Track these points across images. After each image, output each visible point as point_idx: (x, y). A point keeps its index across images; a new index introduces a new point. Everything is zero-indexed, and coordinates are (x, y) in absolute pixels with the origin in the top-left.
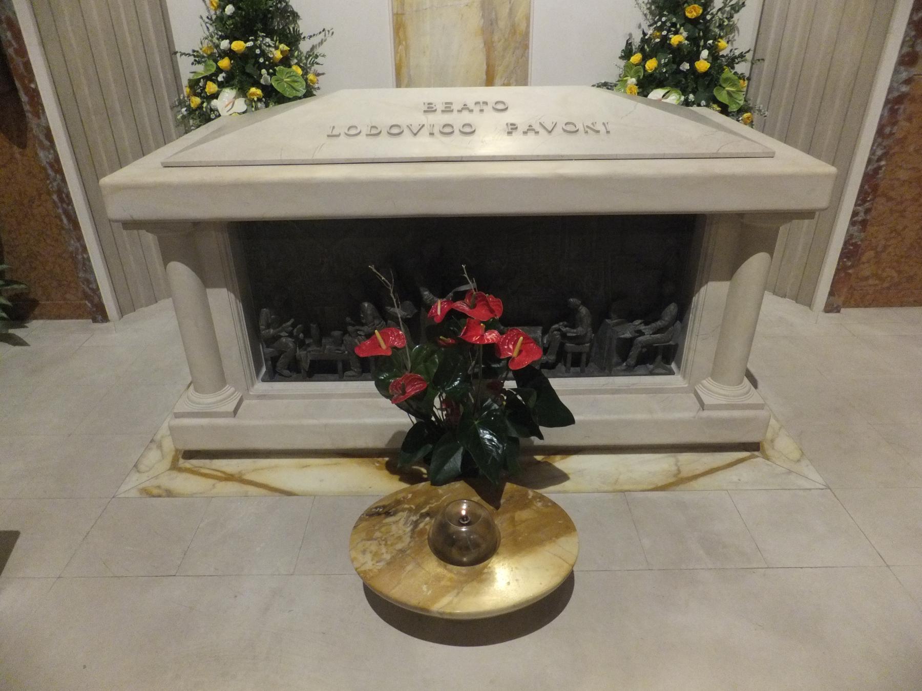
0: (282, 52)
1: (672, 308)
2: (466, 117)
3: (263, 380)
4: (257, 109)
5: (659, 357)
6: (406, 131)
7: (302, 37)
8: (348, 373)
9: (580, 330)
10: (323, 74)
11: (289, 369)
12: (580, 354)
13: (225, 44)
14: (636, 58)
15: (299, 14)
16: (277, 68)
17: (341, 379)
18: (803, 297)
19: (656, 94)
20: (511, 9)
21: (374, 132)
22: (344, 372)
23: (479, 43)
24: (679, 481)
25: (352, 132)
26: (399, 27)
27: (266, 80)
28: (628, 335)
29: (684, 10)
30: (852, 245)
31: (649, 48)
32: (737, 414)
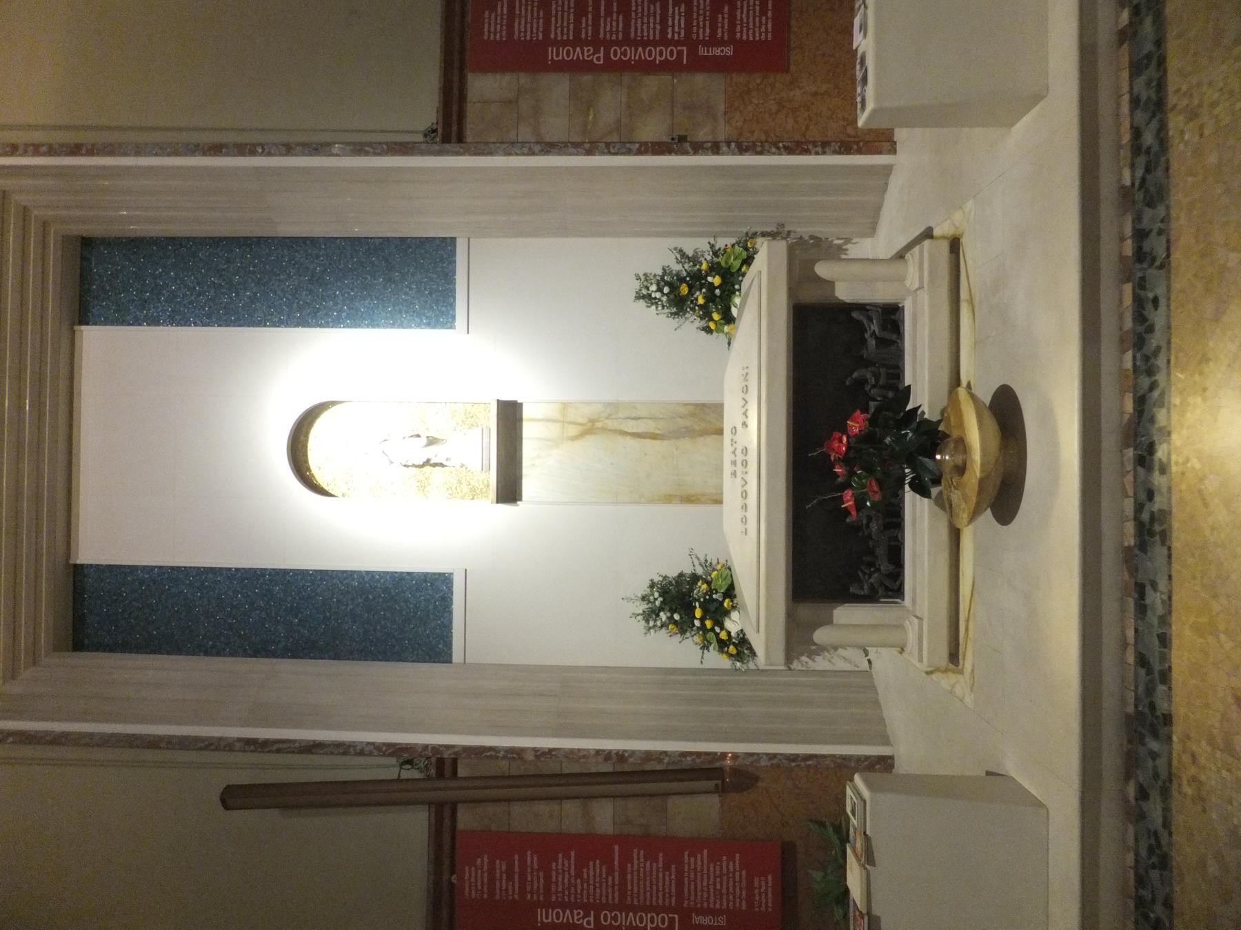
0: (703, 584)
1: (855, 315)
2: (738, 452)
3: (903, 600)
4: (737, 604)
5: (893, 317)
6: (745, 488)
7: (694, 572)
8: (900, 538)
9: (868, 376)
10: (718, 559)
11: (895, 581)
12: (887, 374)
13: (697, 623)
14: (712, 325)
15: (680, 572)
16: (713, 588)
17: (903, 544)
18: (887, 170)
19: (734, 311)
20: (681, 417)
21: (745, 507)
22: (898, 541)
23: (700, 440)
24: (971, 302)
25: (744, 520)
26: (689, 499)
27: (719, 596)
28: (874, 342)
29: (684, 296)
30: (840, 149)
31: (707, 315)
32: (926, 265)
